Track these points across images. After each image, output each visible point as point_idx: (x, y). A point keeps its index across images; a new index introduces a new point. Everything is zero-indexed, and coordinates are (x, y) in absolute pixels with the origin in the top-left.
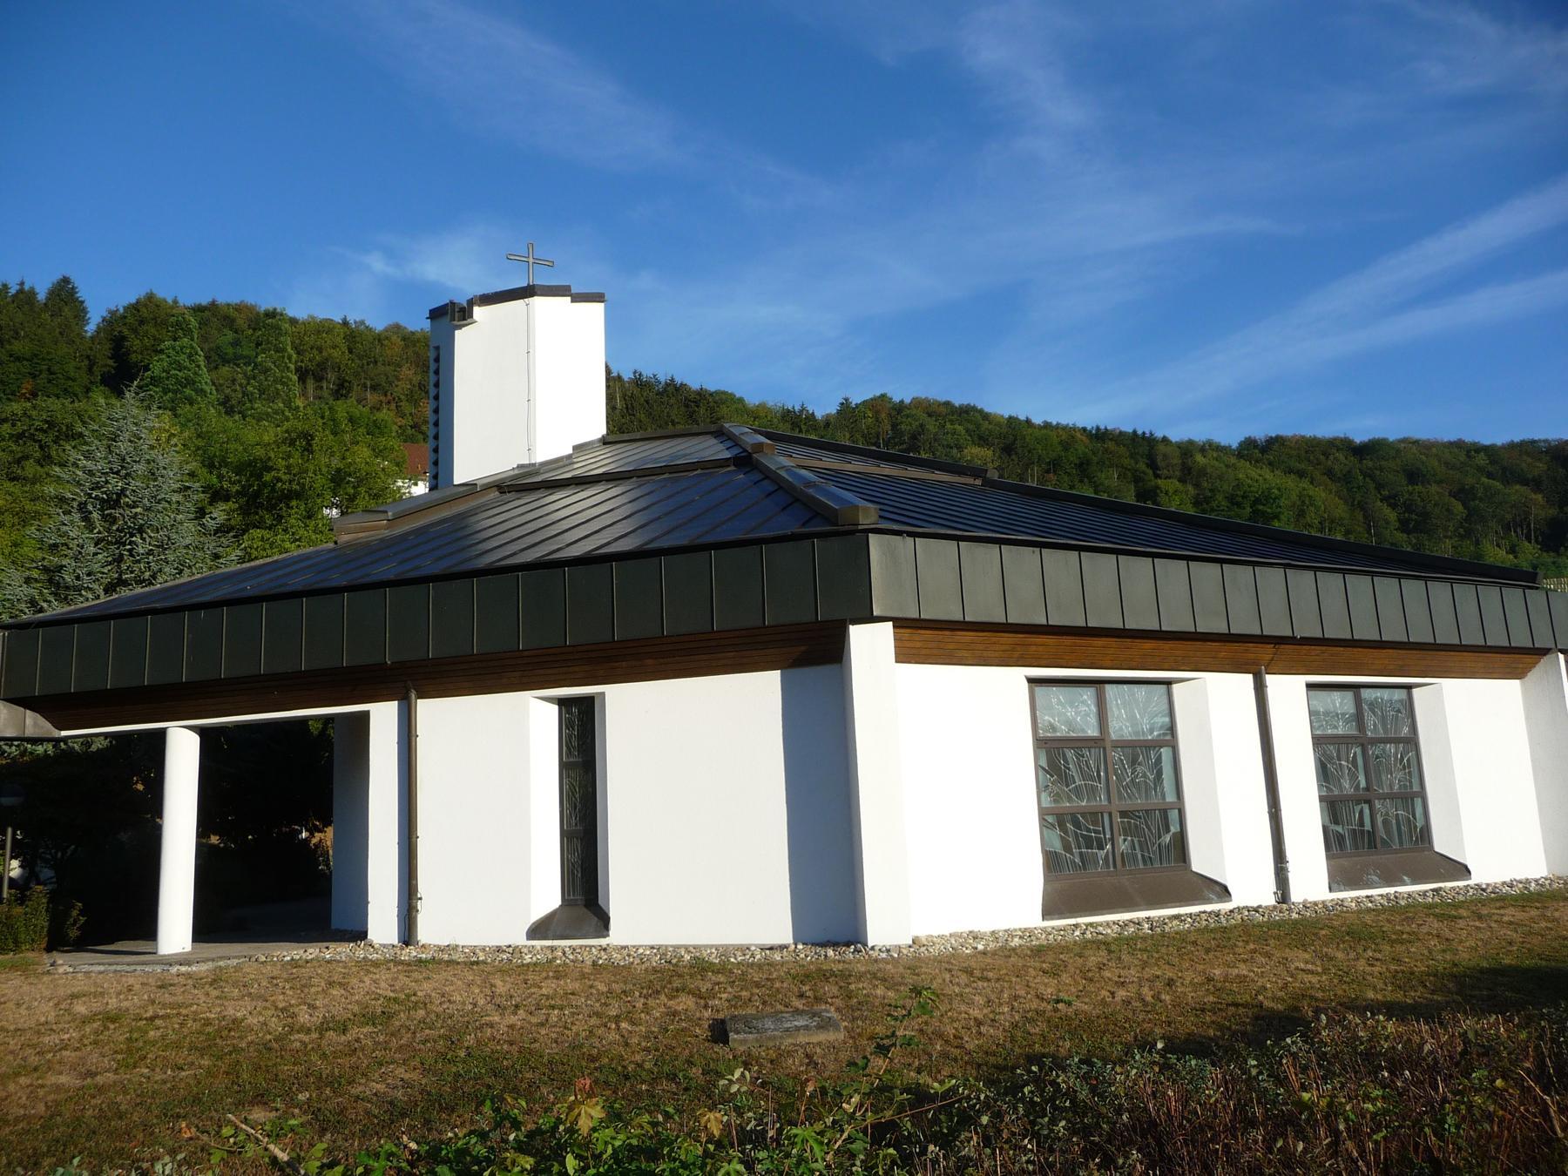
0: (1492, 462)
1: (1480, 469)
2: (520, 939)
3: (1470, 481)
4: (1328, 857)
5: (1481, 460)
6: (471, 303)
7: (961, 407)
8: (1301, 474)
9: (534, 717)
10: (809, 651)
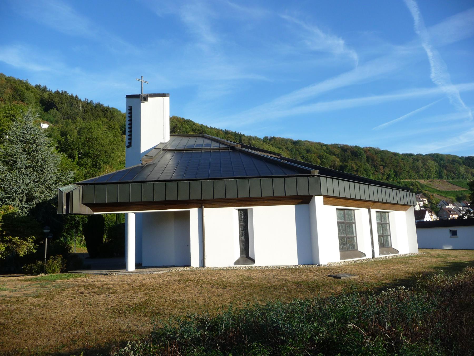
0: (327, 149)
1: (324, 151)
2: (232, 265)
3: (322, 154)
4: (340, 251)
5: (324, 148)
6: (147, 96)
7: (187, 120)
8: (280, 148)
9: (231, 214)
10: (303, 201)
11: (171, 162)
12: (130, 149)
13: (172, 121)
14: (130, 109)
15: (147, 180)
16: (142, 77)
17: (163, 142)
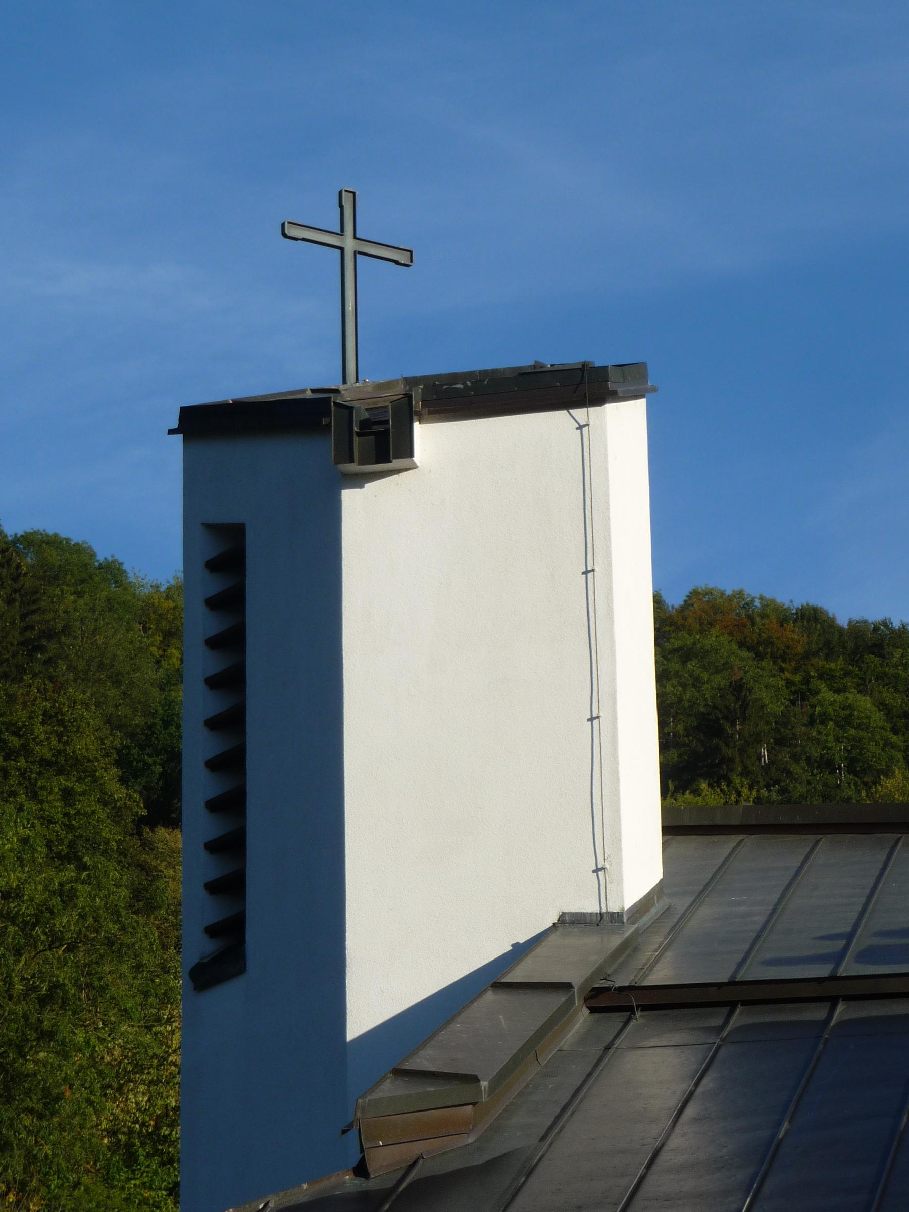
7: (857, 630)
11: (684, 1143)
12: (227, 997)
13: (686, 654)
14: (222, 551)
15: (732, 841)
16: (346, 200)
17: (589, 906)
